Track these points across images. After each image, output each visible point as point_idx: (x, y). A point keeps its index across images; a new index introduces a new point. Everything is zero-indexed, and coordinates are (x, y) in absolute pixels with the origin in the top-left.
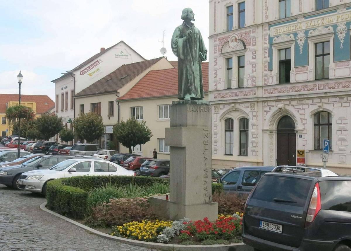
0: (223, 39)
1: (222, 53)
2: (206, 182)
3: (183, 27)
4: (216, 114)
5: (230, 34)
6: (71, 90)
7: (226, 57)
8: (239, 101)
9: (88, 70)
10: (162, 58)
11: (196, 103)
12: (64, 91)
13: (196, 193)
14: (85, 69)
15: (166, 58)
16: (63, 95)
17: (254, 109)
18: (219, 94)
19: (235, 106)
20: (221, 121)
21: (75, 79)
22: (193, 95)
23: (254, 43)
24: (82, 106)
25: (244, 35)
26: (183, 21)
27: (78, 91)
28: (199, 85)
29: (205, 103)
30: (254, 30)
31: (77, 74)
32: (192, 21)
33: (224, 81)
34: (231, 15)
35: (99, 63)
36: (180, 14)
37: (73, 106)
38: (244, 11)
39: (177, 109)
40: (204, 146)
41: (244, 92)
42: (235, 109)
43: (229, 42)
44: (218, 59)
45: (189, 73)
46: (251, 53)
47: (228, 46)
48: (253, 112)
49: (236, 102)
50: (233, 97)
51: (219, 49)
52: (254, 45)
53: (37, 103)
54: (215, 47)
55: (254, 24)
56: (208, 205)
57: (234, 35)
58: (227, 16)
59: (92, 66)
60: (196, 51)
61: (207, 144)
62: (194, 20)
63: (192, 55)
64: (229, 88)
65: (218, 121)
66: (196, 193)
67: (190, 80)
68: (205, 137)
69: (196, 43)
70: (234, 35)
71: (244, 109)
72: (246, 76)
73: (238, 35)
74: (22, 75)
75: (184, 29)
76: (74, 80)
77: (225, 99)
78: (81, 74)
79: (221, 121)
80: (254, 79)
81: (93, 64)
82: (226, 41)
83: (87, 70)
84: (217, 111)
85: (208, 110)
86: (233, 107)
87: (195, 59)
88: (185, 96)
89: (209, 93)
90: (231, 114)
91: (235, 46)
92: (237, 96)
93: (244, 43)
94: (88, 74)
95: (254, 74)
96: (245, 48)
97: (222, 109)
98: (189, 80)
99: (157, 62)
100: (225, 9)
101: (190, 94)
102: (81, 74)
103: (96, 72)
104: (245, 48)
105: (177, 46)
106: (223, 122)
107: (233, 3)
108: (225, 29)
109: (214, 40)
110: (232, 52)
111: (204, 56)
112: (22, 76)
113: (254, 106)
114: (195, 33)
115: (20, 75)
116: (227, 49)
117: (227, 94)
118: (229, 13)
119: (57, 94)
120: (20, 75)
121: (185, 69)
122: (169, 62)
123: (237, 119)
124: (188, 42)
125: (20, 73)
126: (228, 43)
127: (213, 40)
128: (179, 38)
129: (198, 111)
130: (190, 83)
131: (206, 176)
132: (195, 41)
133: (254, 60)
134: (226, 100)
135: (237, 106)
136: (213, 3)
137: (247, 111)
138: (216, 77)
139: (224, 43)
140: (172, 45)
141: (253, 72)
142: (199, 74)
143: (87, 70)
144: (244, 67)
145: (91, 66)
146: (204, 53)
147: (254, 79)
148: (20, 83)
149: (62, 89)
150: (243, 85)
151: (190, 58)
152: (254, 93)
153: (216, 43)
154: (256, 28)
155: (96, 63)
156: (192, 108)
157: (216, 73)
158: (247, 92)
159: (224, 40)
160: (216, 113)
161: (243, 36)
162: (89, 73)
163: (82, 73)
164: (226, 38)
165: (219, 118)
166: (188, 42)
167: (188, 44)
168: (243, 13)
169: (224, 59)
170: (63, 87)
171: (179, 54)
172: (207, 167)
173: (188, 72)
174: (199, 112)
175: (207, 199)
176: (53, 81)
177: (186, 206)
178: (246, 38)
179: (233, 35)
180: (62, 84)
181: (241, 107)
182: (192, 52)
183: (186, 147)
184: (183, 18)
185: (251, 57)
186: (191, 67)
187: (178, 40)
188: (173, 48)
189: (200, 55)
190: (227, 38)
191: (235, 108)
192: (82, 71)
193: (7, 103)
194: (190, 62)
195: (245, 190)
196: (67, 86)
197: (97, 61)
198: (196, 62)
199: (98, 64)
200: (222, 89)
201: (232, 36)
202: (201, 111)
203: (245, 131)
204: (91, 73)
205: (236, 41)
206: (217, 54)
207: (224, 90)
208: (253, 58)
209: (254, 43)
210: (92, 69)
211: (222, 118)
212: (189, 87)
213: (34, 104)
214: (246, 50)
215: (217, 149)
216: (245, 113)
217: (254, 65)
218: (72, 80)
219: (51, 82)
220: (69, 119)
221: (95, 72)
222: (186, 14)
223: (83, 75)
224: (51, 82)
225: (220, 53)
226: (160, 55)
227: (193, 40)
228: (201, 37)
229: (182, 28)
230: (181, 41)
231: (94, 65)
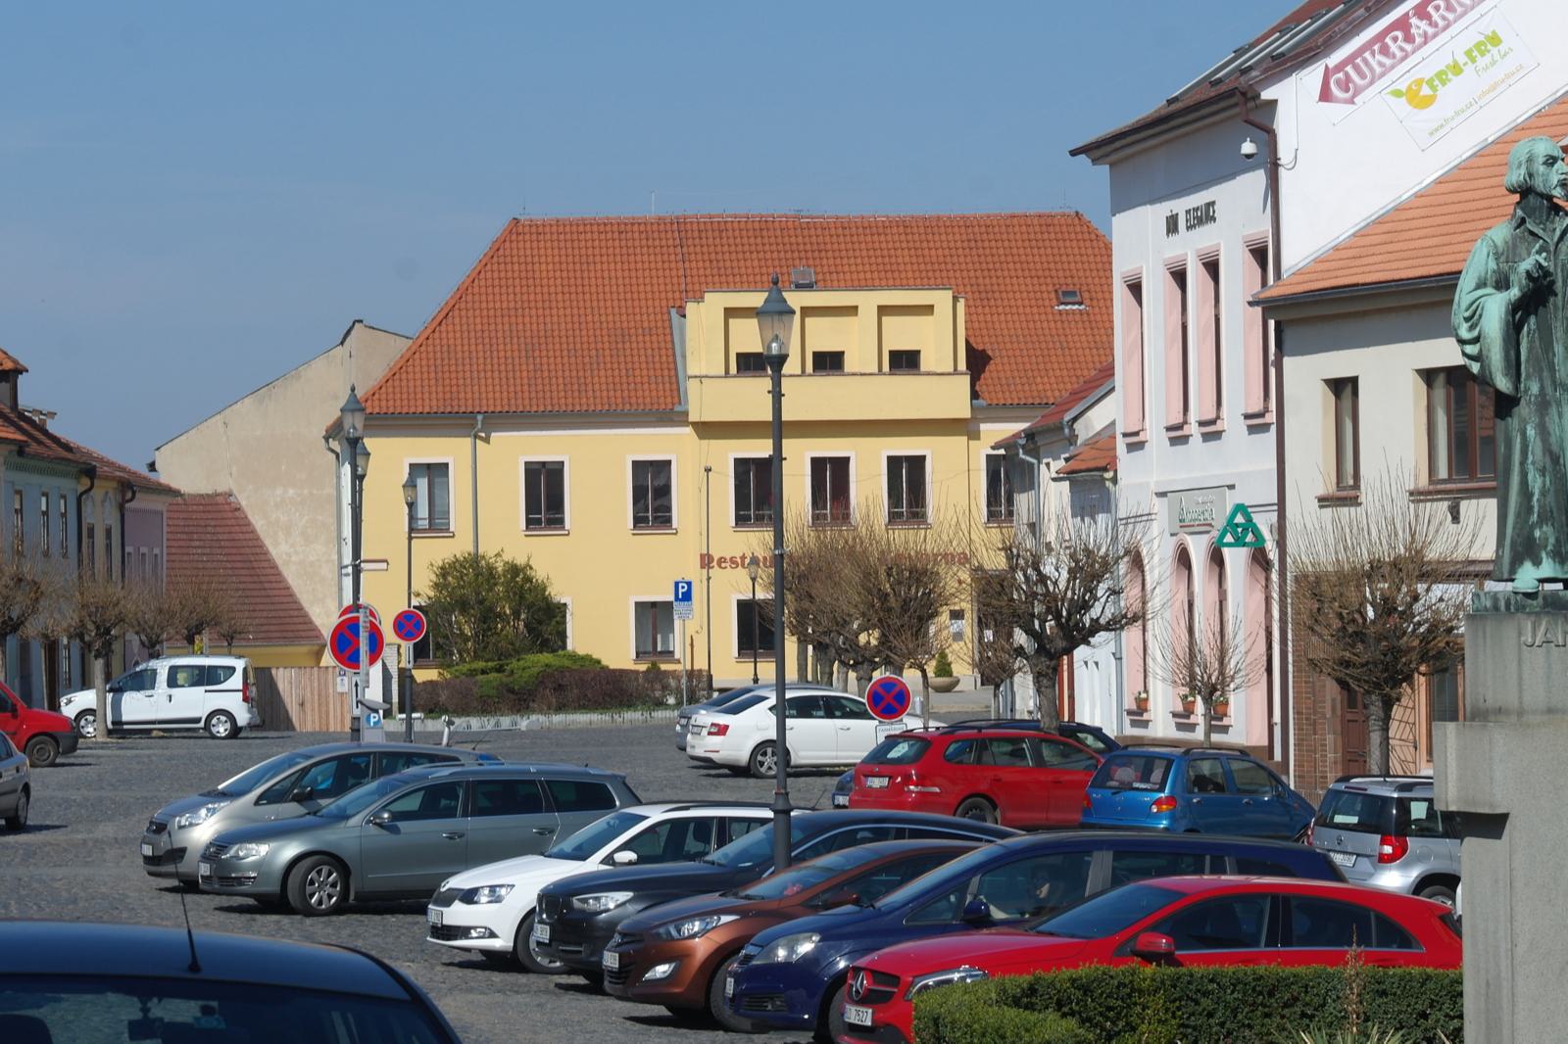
3: (1509, 238)
14: (1367, 46)
27: (1299, 251)
39: (1488, 629)
59: (1426, 16)
75: (1515, 246)
78: (1325, 95)
88: (1515, 573)
98: (1532, 495)
101: (1537, 563)
103: (1469, 69)
121: (1519, 440)
128: (1493, 291)
130: (1536, 510)
149: (1172, 225)
176: (1097, 150)
192: (1340, 67)
195: (893, 833)
196: (1213, 203)
204: (1419, 82)
210: (1426, 39)
212: (1532, 528)
219: (1074, 153)
220: (1229, 509)
221: (1456, 69)
223: (1351, 101)
224: (1074, 153)
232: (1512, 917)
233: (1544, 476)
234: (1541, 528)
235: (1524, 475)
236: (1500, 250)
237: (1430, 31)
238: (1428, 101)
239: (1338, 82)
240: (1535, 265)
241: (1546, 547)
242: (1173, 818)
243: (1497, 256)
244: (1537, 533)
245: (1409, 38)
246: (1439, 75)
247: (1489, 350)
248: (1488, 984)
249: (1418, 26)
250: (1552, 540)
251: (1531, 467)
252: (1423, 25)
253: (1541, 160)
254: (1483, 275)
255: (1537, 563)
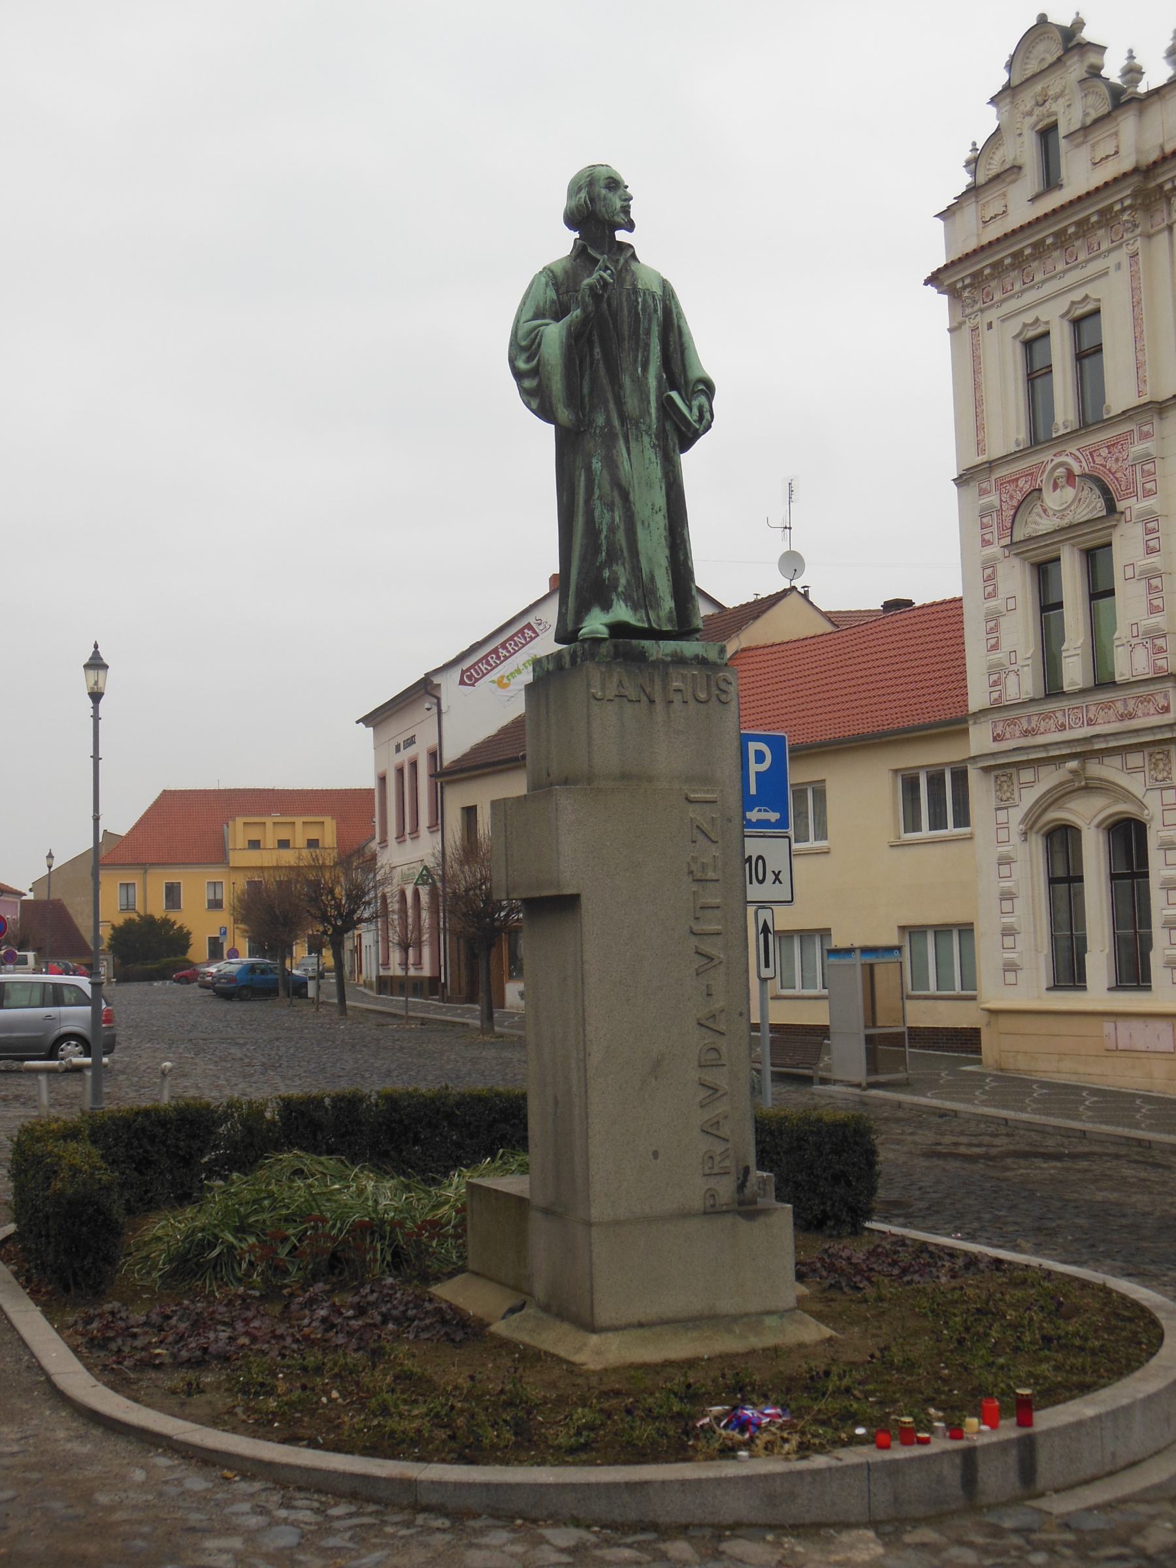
0: (1017, 480)
1: (1015, 539)
2: (716, 1090)
4: (1006, 808)
5: (1047, 457)
6: (428, 751)
7: (1032, 557)
8: (1097, 747)
9: (490, 665)
10: (784, 594)
11: (641, 657)
12: (405, 756)
13: (656, 1154)
14: (480, 661)
15: (805, 596)
16: (400, 771)
17: (1165, 774)
18: (1013, 722)
19: (1084, 769)
20: (1026, 840)
21: (439, 705)
22: (622, 612)
23: (1148, 486)
24: (470, 813)
25: (1104, 452)
26: (577, 235)
27: (450, 754)
28: (664, 562)
29: (696, 657)
30: (1145, 429)
31: (449, 685)
32: (621, 236)
33: (1029, 662)
34: (1045, 374)
35: (534, 631)
36: (560, 203)
37: (438, 821)
38: (1098, 349)
40: (695, 887)
41: (1119, 705)
42: (1083, 783)
43: (1040, 490)
44: (1000, 567)
45: (600, 498)
46: (1139, 529)
47: (1038, 509)
48: (1162, 789)
49: (1086, 752)
50: (1071, 728)
51: (1002, 527)
52: (1148, 494)
53: (342, 820)
54: (985, 520)
55: (1145, 399)
56: (728, 1220)
57: (1063, 459)
58: (1028, 380)
60: (640, 385)
61: (711, 875)
62: (630, 226)
63: (620, 403)
64: (1053, 689)
65: (1016, 839)
66: (656, 1154)
67: (603, 536)
68: (700, 837)
69: (642, 344)
70: (1063, 459)
71: (1122, 780)
72: (1122, 632)
73: (1076, 458)
74: (106, 661)
76: (435, 709)
77: (1041, 740)
78: (462, 682)
79: (1026, 840)
80: (1160, 642)
81: (511, 638)
82: (1027, 488)
83: (488, 663)
84: (1008, 794)
85: (716, 692)
86: (1073, 772)
87: (637, 424)
89: (971, 722)
90: (1068, 806)
91: (1069, 506)
92: (1090, 722)
93: (1106, 492)
94: (493, 682)
95: (1157, 620)
96: (1111, 507)
97: (1030, 784)
98: (600, 531)
99: (764, 612)
100: (1019, 349)
101: (606, 607)
102: (462, 682)
104: (1111, 507)
105: (535, 362)
106: (1037, 844)
107: (1047, 323)
108: (1023, 435)
109: (980, 490)
110: (1055, 531)
111: (690, 409)
112: (107, 667)
113: (1165, 765)
114: (635, 290)
115: (96, 663)
116: (1040, 523)
117: (1046, 717)
118: (1038, 365)
119: (381, 770)
120: (96, 663)
121: (583, 478)
122: (826, 615)
123: (1098, 826)
124: (596, 338)
125: (96, 655)
126: (1036, 494)
127: (973, 489)
129: (658, 699)
130: (604, 548)
131: (714, 1055)
132: (635, 333)
133: (1154, 559)
134: (1045, 746)
135: (1095, 769)
136: (966, 331)
137: (1135, 784)
138: (995, 647)
139: (1019, 497)
140: (512, 361)
141: (1154, 610)
142: (660, 500)
143: (488, 663)
144: (1111, 593)
145: (503, 645)
146: (694, 392)
147: (1160, 642)
148: (96, 696)
149: (398, 749)
150: (1113, 674)
151: (608, 421)
152: (1162, 702)
153: (986, 500)
154: (1155, 421)
155: (523, 634)
156: (615, 680)
157: (995, 629)
158: (1131, 703)
159: (1021, 483)
160: (1003, 804)
161: (1098, 460)
162: (494, 675)
163: (468, 679)
164: (1030, 474)
165: (1016, 827)
166: (596, 338)
167: (597, 350)
168: (1094, 359)
169: (1027, 566)
170: (401, 740)
171: (551, 403)
172: (719, 1003)
173: (597, 493)
174: (659, 706)
175: (726, 1189)
177: (595, 1232)
178: (1114, 467)
179: (1057, 460)
180: (398, 729)
181: (1108, 770)
182: (621, 386)
183: (583, 900)
184: (573, 220)
185: (1141, 549)
186: (611, 464)
187: (542, 328)
188: (518, 375)
189: (667, 407)
190: (1032, 474)
191: (1086, 779)
192: (468, 670)
193: (225, 827)
194: (609, 439)
197: (529, 627)
198: (646, 439)
199: (532, 639)
200: (1025, 697)
201: (1054, 463)
202: (677, 698)
203: (1132, 876)
204: (502, 677)
205: (1070, 485)
206: (995, 550)
207: (1032, 700)
208: (1150, 551)
209: (1148, 486)
210: (506, 658)
211: (1031, 828)
212: (600, 569)
213: (330, 824)
214: (1117, 516)
215: (1018, 962)
216: (1127, 795)
217: (1155, 582)
218: (428, 709)
219: (358, 722)
222: (583, 194)
223: (473, 685)
224: (358, 722)
225: (1007, 541)
226: (780, 584)
227: (626, 327)
228: (680, 315)
229: (566, 272)
230: (554, 333)
231: (516, 645)
232: (584, 1019)
233: (613, 511)
234: (610, 567)
235: (589, 513)
236: (560, 279)
237: (508, 654)
238: (506, 686)
239: (467, 676)
240: (598, 281)
241: (616, 588)
242: (1011, 1320)
243: (557, 286)
244: (606, 574)
245: (498, 658)
246: (511, 674)
247: (549, 379)
248: (556, 1102)
249: (503, 652)
250: (623, 581)
251: (598, 503)
252: (505, 652)
253: (602, 183)
254: (541, 304)
255: (606, 607)
